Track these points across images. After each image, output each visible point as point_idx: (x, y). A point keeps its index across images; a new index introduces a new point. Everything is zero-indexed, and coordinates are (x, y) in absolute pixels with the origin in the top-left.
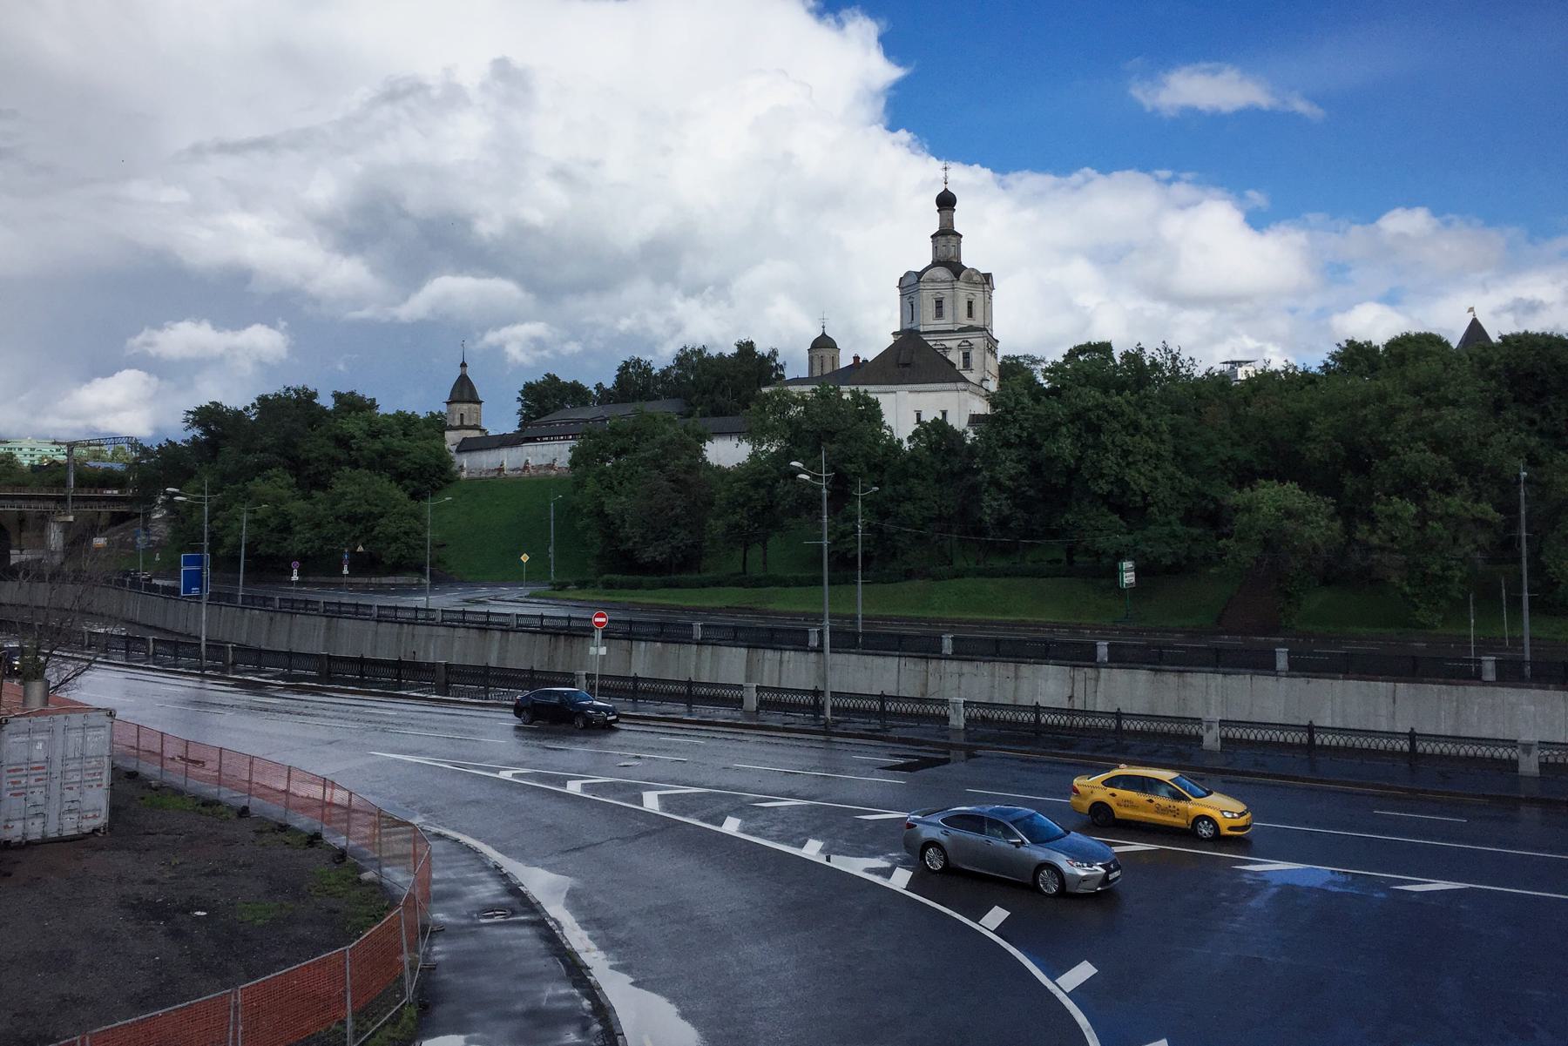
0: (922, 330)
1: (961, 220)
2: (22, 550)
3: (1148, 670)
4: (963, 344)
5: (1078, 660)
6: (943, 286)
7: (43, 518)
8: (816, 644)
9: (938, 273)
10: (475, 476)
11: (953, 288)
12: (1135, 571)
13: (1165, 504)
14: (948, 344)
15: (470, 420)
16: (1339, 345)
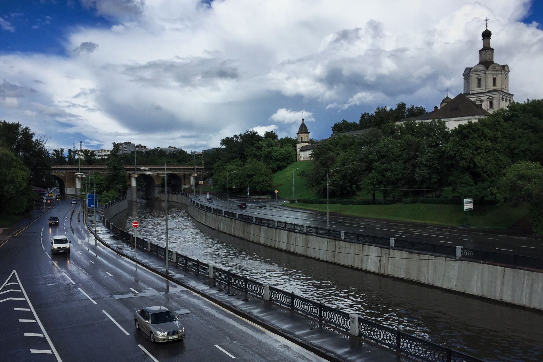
0: (471, 93)
1: (494, 42)
2: (185, 185)
3: (407, 251)
4: (490, 98)
6: (481, 73)
7: (190, 175)
9: (479, 67)
10: (305, 159)
11: (485, 73)
12: (473, 202)
13: (492, 172)
14: (482, 98)
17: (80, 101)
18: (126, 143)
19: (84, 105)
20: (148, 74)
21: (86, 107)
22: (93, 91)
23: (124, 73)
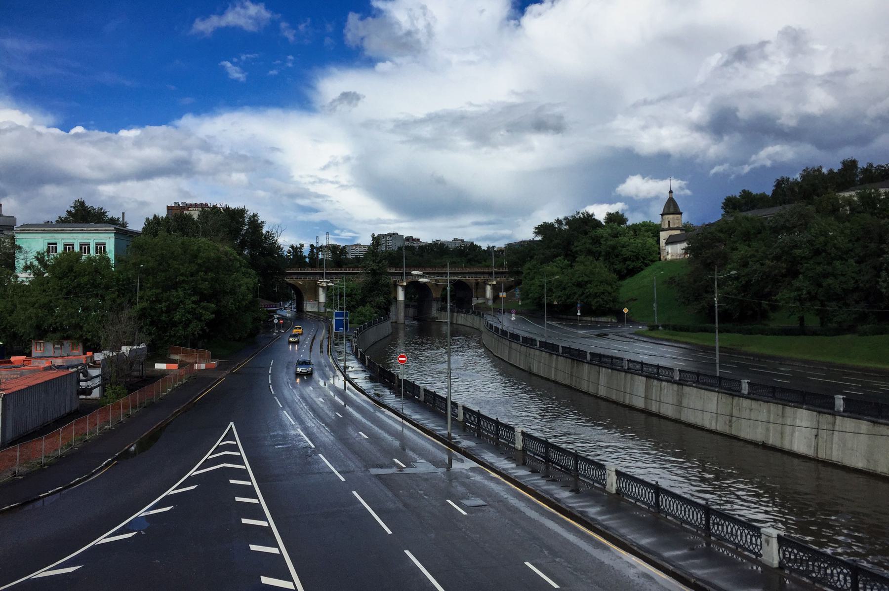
5: (824, 408)
7: (485, 283)
8: (678, 378)
15: (674, 224)
16: (81, 199)
17: (329, 175)
18: (390, 235)
19: (334, 180)
20: (426, 131)
21: (337, 183)
22: (347, 159)
23: (392, 131)
